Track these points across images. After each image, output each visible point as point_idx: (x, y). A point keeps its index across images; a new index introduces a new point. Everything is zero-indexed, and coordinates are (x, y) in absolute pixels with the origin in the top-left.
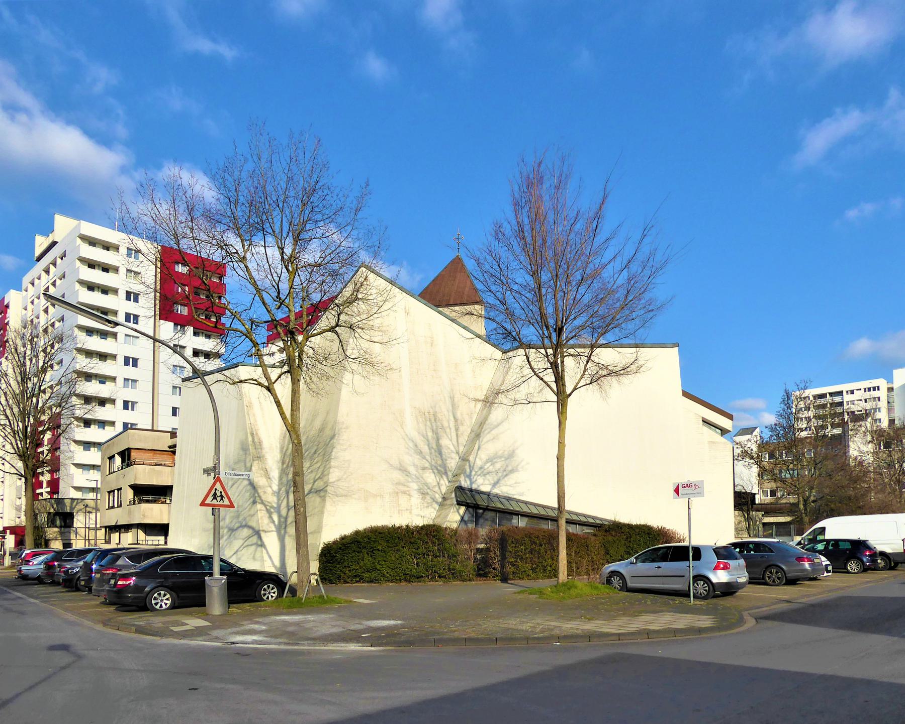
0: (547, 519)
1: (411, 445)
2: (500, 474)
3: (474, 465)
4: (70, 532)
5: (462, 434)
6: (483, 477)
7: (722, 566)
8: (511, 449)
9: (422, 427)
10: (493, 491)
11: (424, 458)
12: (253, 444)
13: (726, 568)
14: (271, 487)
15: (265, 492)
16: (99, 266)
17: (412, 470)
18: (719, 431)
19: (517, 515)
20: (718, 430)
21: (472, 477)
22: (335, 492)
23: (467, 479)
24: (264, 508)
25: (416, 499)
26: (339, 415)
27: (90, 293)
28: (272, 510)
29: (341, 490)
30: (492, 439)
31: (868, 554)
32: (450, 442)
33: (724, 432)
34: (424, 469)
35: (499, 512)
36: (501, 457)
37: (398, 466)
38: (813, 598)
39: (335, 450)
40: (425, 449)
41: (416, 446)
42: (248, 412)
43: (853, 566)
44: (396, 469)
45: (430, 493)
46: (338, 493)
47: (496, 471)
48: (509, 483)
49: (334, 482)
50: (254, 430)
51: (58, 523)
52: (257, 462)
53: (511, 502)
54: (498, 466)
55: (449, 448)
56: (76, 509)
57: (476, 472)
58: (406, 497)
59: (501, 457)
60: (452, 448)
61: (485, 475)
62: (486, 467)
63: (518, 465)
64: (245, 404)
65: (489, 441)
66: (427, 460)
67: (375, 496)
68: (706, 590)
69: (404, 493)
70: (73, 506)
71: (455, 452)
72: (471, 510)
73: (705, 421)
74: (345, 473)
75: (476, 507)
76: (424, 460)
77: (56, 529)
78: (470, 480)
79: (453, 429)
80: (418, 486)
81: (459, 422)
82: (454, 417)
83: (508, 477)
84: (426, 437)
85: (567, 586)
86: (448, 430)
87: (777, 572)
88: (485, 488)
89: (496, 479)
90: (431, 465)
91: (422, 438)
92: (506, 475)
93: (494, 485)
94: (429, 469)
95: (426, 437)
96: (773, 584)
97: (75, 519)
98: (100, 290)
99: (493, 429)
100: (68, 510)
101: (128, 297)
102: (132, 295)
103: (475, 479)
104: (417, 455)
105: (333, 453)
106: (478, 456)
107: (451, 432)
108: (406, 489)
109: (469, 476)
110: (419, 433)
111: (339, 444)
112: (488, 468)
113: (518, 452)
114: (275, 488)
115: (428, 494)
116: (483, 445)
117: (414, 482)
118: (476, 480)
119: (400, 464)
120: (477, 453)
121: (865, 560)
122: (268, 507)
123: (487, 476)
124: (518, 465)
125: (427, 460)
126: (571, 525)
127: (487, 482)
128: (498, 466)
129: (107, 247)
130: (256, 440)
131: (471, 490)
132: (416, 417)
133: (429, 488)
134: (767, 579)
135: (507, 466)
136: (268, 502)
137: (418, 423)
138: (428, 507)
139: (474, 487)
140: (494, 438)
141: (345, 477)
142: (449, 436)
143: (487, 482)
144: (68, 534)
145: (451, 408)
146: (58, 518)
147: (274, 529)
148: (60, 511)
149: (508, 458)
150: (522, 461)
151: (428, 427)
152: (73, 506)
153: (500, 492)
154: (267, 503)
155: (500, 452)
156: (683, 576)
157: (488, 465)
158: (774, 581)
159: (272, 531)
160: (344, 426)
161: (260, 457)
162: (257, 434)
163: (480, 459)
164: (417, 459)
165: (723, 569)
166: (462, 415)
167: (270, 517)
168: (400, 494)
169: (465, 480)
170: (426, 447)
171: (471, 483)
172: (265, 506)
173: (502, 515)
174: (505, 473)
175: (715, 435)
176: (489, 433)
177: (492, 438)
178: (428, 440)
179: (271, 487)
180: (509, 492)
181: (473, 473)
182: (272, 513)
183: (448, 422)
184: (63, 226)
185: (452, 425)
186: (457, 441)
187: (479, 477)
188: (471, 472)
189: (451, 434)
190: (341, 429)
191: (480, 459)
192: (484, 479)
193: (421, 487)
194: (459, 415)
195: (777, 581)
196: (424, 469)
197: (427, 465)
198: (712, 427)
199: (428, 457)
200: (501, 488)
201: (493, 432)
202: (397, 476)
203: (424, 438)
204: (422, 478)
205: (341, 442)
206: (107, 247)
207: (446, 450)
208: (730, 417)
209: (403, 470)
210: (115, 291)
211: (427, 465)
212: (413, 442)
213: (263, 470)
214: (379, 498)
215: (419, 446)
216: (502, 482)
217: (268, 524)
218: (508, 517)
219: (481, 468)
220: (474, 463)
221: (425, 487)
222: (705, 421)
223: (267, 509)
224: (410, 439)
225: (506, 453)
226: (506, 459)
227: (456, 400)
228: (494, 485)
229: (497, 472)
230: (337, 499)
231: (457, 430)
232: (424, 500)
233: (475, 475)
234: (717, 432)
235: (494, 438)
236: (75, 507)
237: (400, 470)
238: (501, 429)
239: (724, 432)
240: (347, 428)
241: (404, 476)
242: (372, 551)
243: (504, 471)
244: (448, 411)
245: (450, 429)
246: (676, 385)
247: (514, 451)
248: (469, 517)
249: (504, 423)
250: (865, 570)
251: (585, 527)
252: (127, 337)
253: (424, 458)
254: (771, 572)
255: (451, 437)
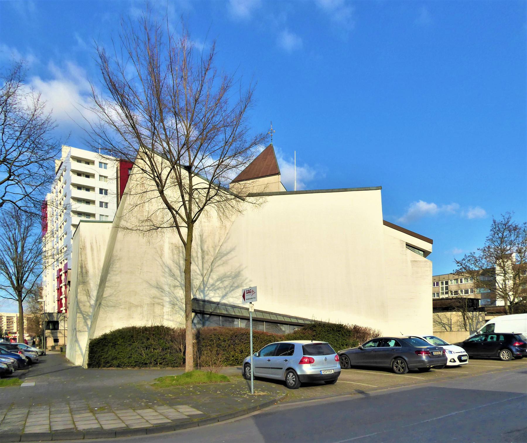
0: (263, 321)
1: (167, 270)
2: (228, 289)
3: (207, 283)
4: (57, 333)
5: (207, 262)
6: (214, 292)
7: (306, 360)
8: (237, 270)
9: (176, 257)
10: (222, 301)
11: (177, 279)
12: (81, 274)
13: (310, 362)
14: (89, 302)
15: (84, 305)
16: (83, 174)
17: (166, 288)
18: (422, 253)
19: (238, 318)
20: (420, 252)
21: (205, 292)
22: (107, 304)
23: (201, 293)
24: (81, 316)
25: (167, 308)
26: (115, 250)
27: (79, 191)
28: (87, 317)
29: (111, 302)
30: (222, 264)
31: (517, 345)
32: (197, 267)
33: (426, 254)
34: (175, 287)
35: (222, 316)
36: (229, 277)
37: (156, 285)
38: (385, 390)
39: (109, 275)
40: (177, 272)
41: (170, 270)
42: (81, 252)
43: (504, 355)
44: (154, 287)
45: (178, 304)
46: (109, 305)
47: (224, 287)
48: (234, 296)
49: (107, 297)
50: (83, 264)
51: (51, 327)
52: (82, 285)
53: (235, 309)
54: (226, 283)
55: (196, 272)
56: (60, 319)
57: (208, 288)
58: (160, 307)
59: (229, 277)
60: (198, 272)
61: (215, 290)
62: (217, 284)
63: (242, 283)
64: (80, 247)
65: (220, 265)
66: (178, 281)
67: (137, 306)
68: (294, 381)
69: (159, 304)
70: (58, 317)
71: (200, 274)
72: (199, 315)
73: (409, 246)
74: (115, 291)
75: (203, 313)
76: (176, 281)
77: (49, 331)
78: (204, 294)
79: (200, 258)
80: (170, 299)
81: (205, 252)
82: (202, 250)
83: (234, 291)
84: (178, 264)
85: (189, 375)
86: (196, 259)
87: (402, 363)
88: (216, 300)
89: (224, 293)
90: (181, 284)
91: (176, 265)
92: (233, 290)
93: (223, 297)
94: (180, 287)
95: (178, 264)
96: (399, 372)
97: (60, 325)
98: (85, 189)
99: (224, 256)
100: (55, 319)
101: (101, 192)
102: (103, 191)
103: (207, 293)
104: (171, 277)
105: (108, 277)
106: (211, 277)
107: (198, 260)
108: (160, 301)
109: (203, 291)
110: (173, 261)
111: (112, 270)
112: (218, 285)
113: (243, 273)
114: (93, 302)
115: (177, 304)
116: (215, 268)
117: (166, 296)
118: (208, 294)
119: (157, 284)
120: (210, 275)
121: (514, 350)
122: (85, 316)
123: (218, 291)
124: (242, 283)
125: (178, 281)
126: (284, 325)
127: (217, 295)
128: (226, 283)
129: (88, 162)
130: (84, 271)
131: (204, 301)
132: (172, 250)
133: (178, 300)
134: (395, 367)
135: (234, 283)
136: (85, 312)
137: (173, 255)
138: (176, 313)
139: (207, 298)
140: (224, 263)
141: (115, 293)
142: (197, 263)
143: (217, 295)
144: (55, 334)
145: (199, 243)
146: (50, 324)
147: (86, 330)
148: (51, 320)
149: (235, 277)
150: (246, 279)
151: (180, 258)
152: (58, 317)
153: (227, 302)
154: (84, 313)
155: (229, 273)
156: (282, 369)
157: (218, 283)
158: (399, 370)
159: (86, 331)
160: (118, 258)
161: (85, 282)
162: (85, 267)
163: (212, 278)
164: (170, 280)
165: (307, 363)
166: (208, 247)
167: (85, 322)
168: (156, 305)
169: (200, 294)
170: (178, 271)
171: (205, 296)
172: (83, 314)
173: (224, 318)
174: (232, 289)
175: (420, 257)
176: (220, 259)
177: (222, 263)
178: (180, 267)
179: (89, 302)
180: (234, 302)
181: (206, 289)
182: (87, 319)
183: (197, 253)
184: (66, 151)
185: (200, 255)
186: (203, 267)
187: (211, 292)
188: (204, 288)
189: (198, 262)
190: (115, 260)
191: (212, 278)
192: (215, 293)
193: (172, 299)
194: (205, 248)
195: (402, 370)
196: (175, 287)
197: (178, 284)
198: (416, 250)
199: (179, 279)
200: (229, 299)
201: (224, 259)
202: (154, 292)
203: (177, 264)
204: (173, 293)
205: (114, 269)
206: (88, 162)
207: (194, 273)
208: (430, 241)
209: (159, 288)
210: (93, 189)
211: (178, 284)
212: (168, 268)
213: (85, 291)
214: (139, 308)
215: (173, 271)
216: (230, 295)
217: (83, 327)
218: (230, 319)
219: (212, 285)
220: (207, 282)
221: (175, 300)
222: (408, 245)
223: (84, 317)
224: (166, 266)
225: (233, 273)
226: (233, 278)
227: (204, 237)
228: (223, 297)
229: (225, 288)
230: (108, 309)
231: (203, 258)
232: (173, 309)
233: (207, 290)
234: (420, 254)
235: (224, 263)
236: (59, 318)
237: (157, 288)
238: (229, 256)
239: (426, 254)
240: (119, 259)
241: (159, 292)
242: (115, 344)
243: (232, 286)
244: (197, 245)
245: (198, 258)
246: (379, 218)
247: (239, 272)
248: (198, 321)
249: (232, 252)
250: (517, 358)
251: (295, 327)
252: (101, 216)
253: (177, 279)
254: (397, 363)
255: (198, 264)
